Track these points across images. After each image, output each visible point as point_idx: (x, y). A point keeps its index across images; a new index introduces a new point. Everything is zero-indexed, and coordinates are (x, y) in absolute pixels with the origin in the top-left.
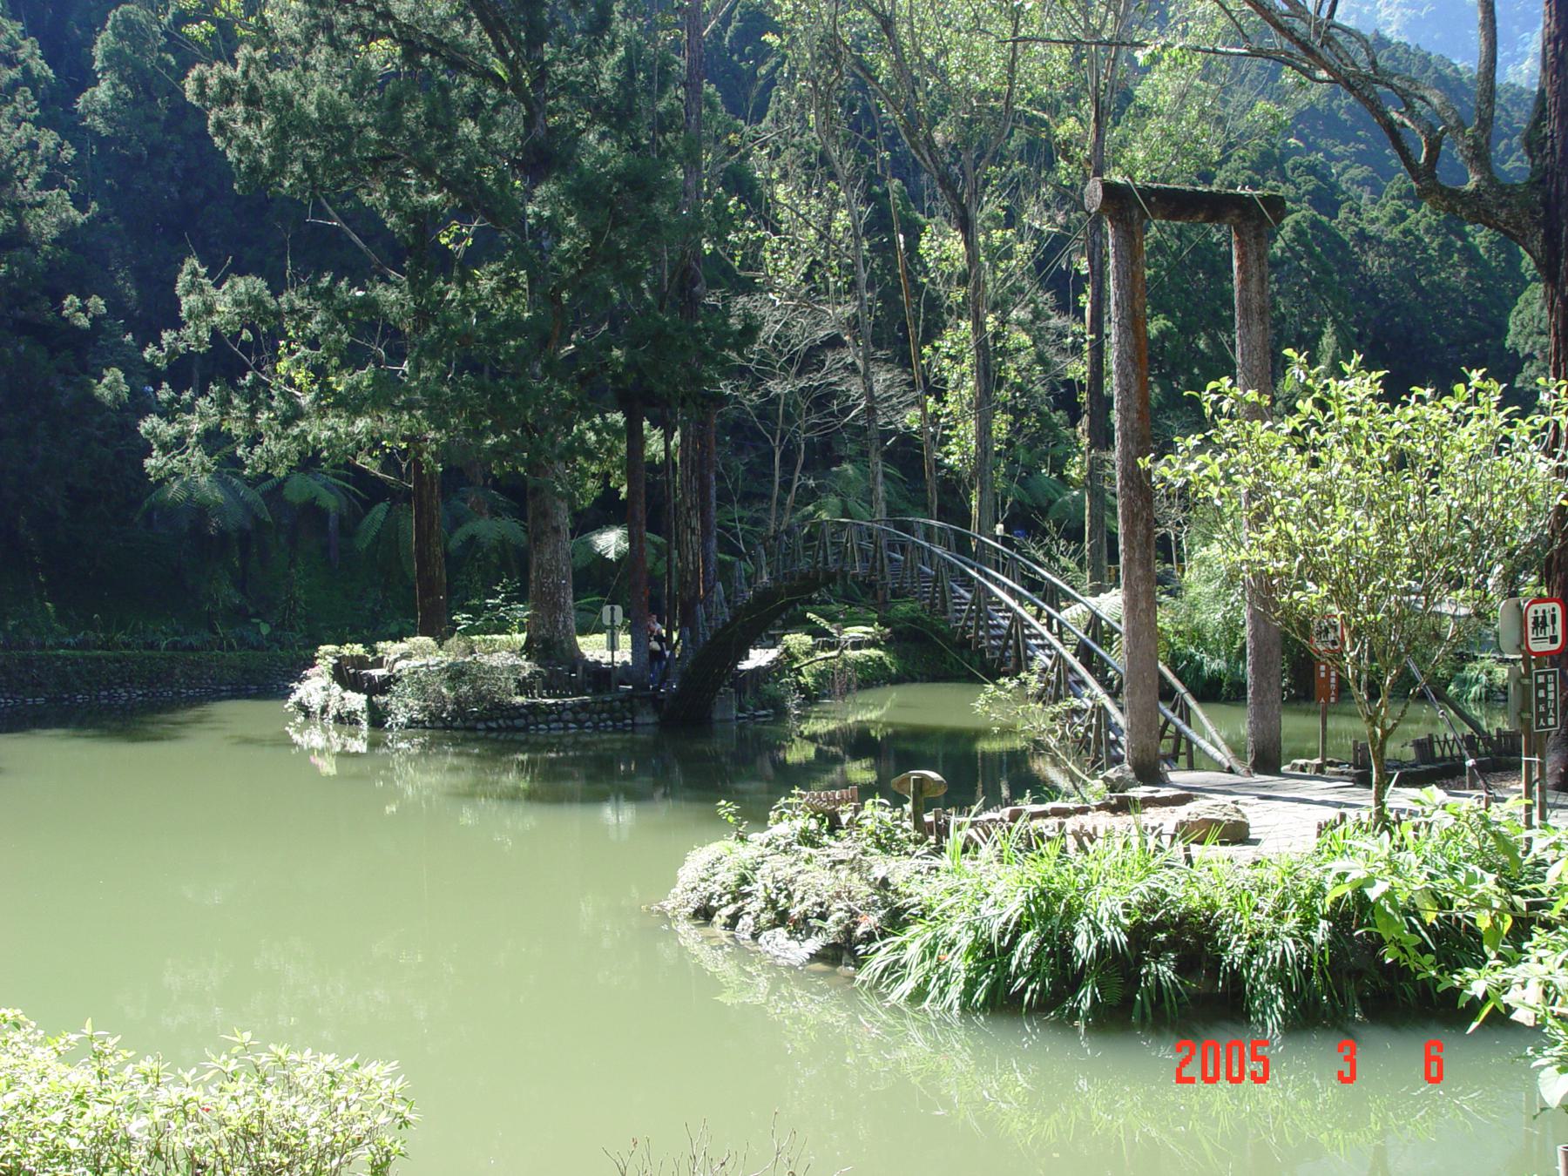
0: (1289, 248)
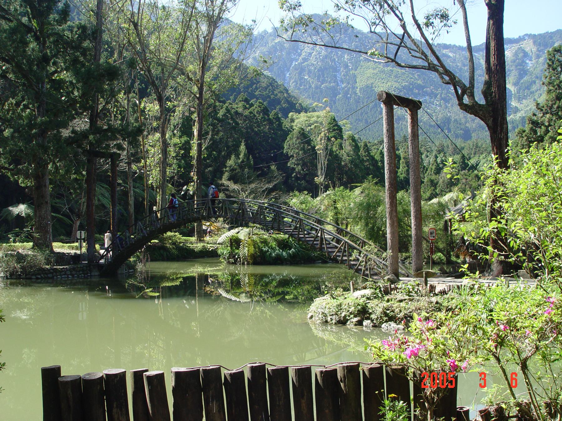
0: (224, 115)
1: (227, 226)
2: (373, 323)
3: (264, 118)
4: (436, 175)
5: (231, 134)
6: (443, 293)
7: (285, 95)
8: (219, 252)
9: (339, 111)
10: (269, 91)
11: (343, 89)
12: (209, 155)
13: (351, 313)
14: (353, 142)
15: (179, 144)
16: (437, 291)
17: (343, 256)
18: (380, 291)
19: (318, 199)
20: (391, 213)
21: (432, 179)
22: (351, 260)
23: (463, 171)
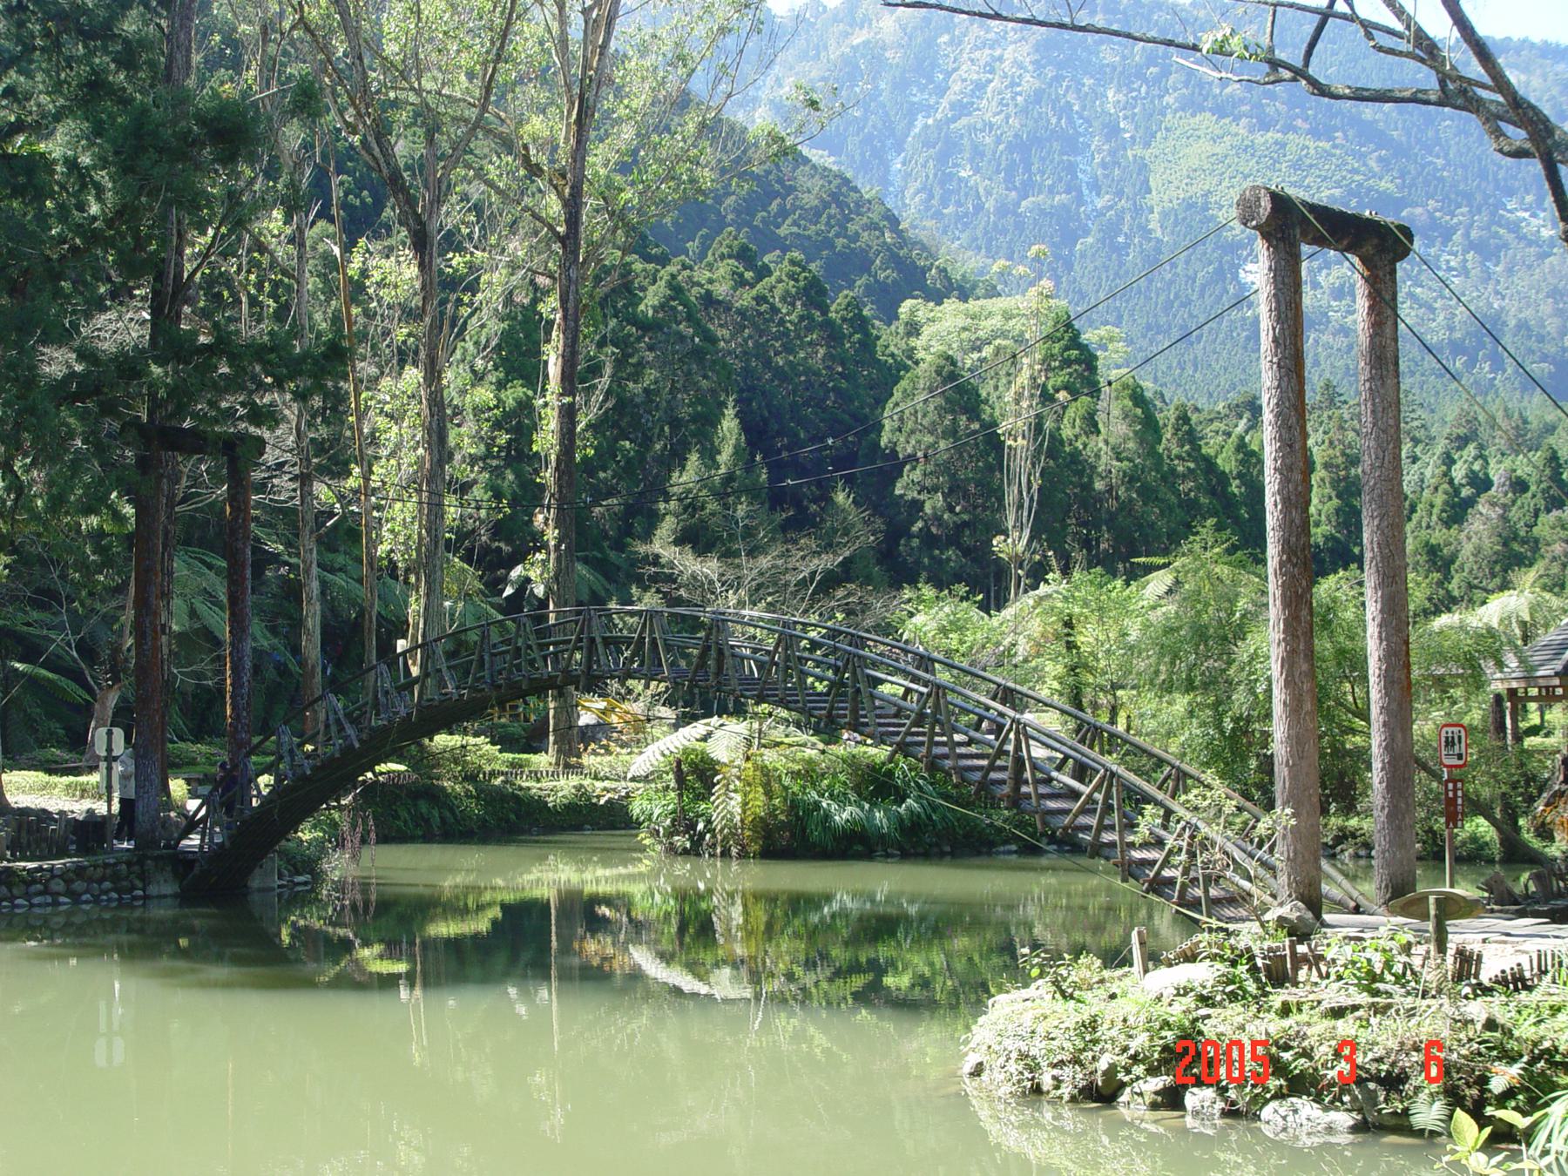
0: (662, 306)
1: (667, 713)
2: (1226, 1100)
3: (810, 317)
4: (1449, 528)
5: (689, 374)
6: (1516, 982)
7: (888, 236)
8: (636, 808)
9: (1083, 296)
10: (828, 223)
11: (1101, 214)
12: (606, 454)
13: (1135, 1058)
14: (1136, 405)
15: (490, 409)
16: (1487, 975)
17: (1102, 827)
18: (1254, 970)
19: (1008, 613)
20: (1289, 662)
21: (1433, 541)
22: (1132, 845)
23: (1555, 513)
